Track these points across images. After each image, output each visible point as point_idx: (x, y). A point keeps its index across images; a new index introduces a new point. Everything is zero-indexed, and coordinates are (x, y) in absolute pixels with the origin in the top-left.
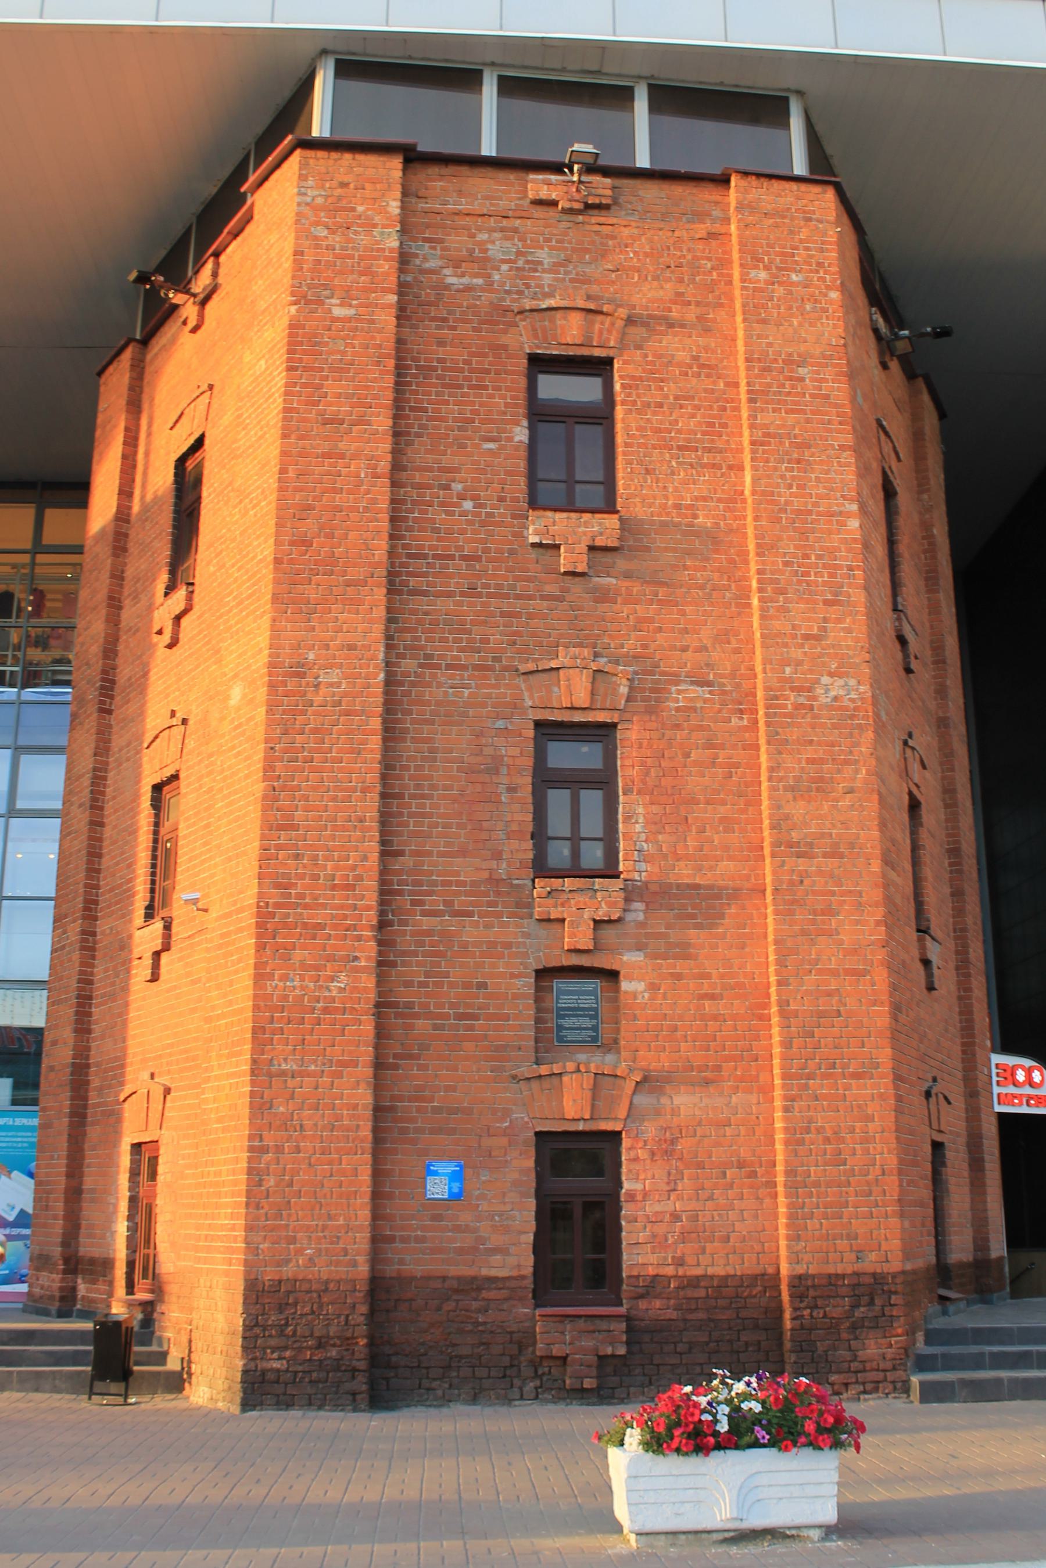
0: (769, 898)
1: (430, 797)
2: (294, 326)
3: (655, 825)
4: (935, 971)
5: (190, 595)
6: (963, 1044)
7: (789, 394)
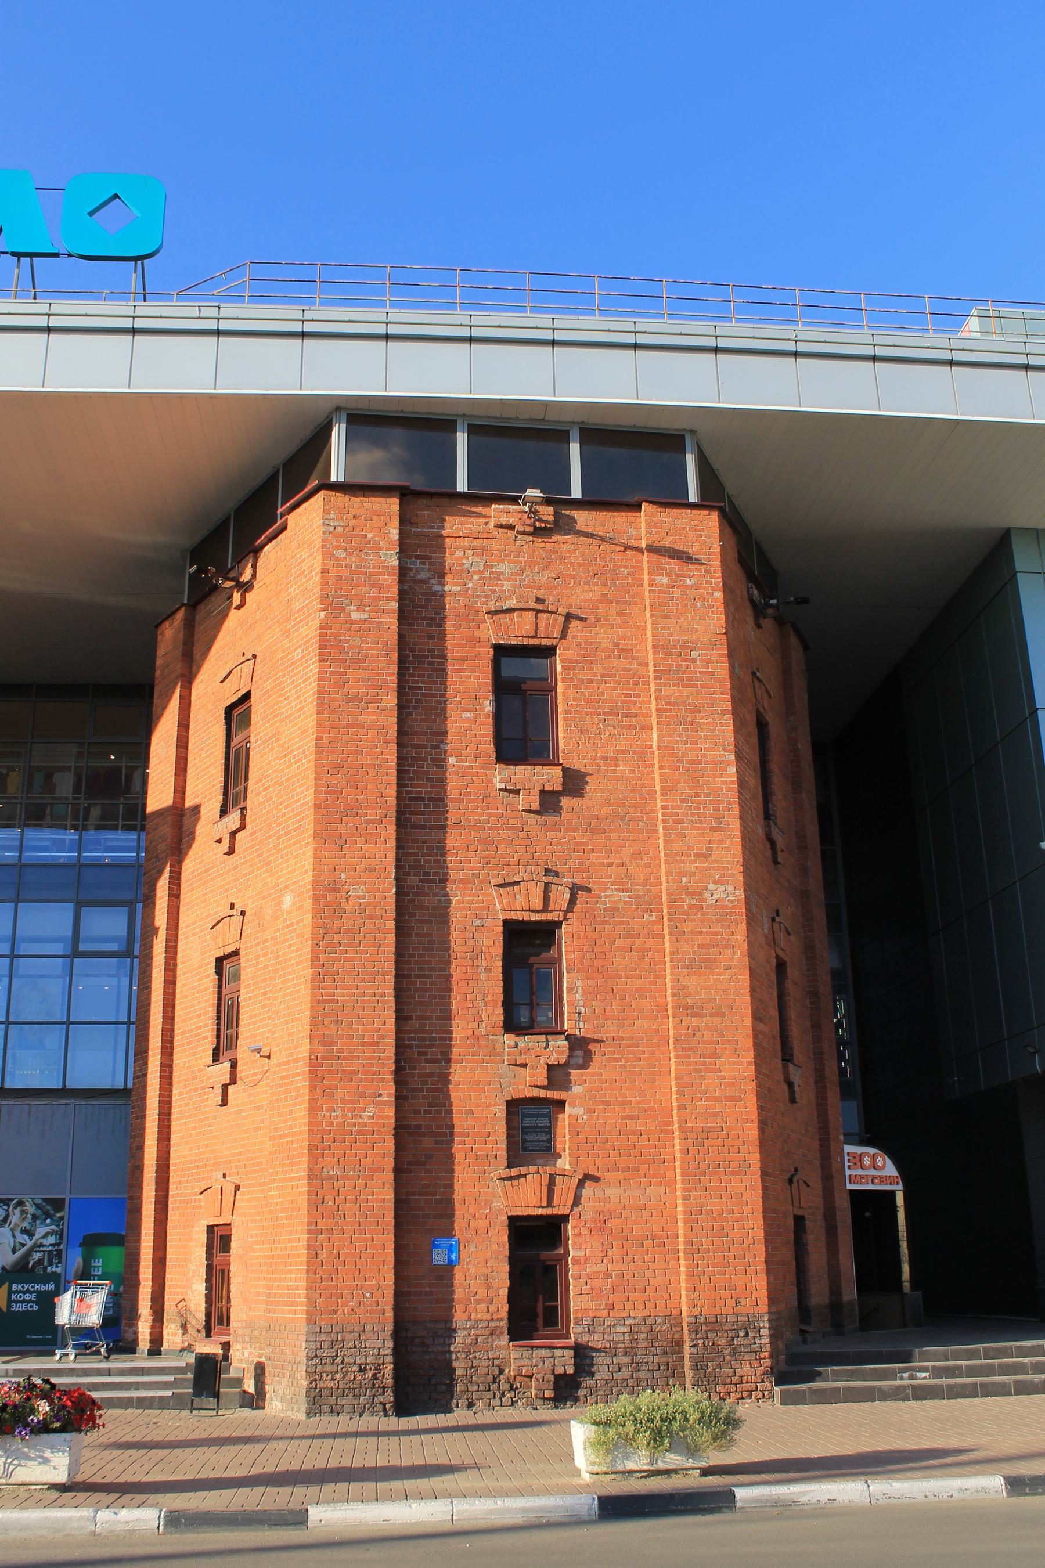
0: (672, 1046)
1: (430, 977)
2: (323, 628)
3: (591, 994)
4: (796, 1088)
5: (243, 817)
6: (820, 1140)
7: (684, 672)
